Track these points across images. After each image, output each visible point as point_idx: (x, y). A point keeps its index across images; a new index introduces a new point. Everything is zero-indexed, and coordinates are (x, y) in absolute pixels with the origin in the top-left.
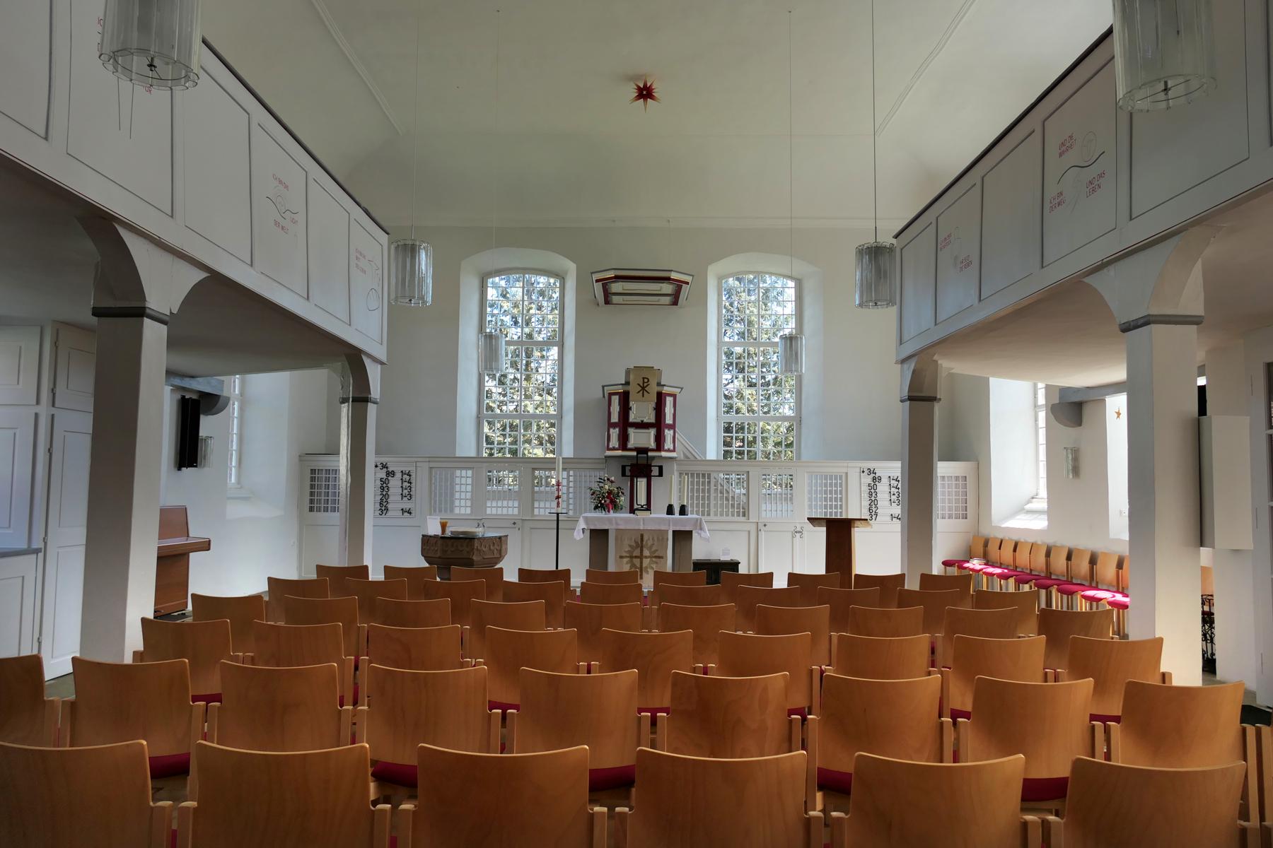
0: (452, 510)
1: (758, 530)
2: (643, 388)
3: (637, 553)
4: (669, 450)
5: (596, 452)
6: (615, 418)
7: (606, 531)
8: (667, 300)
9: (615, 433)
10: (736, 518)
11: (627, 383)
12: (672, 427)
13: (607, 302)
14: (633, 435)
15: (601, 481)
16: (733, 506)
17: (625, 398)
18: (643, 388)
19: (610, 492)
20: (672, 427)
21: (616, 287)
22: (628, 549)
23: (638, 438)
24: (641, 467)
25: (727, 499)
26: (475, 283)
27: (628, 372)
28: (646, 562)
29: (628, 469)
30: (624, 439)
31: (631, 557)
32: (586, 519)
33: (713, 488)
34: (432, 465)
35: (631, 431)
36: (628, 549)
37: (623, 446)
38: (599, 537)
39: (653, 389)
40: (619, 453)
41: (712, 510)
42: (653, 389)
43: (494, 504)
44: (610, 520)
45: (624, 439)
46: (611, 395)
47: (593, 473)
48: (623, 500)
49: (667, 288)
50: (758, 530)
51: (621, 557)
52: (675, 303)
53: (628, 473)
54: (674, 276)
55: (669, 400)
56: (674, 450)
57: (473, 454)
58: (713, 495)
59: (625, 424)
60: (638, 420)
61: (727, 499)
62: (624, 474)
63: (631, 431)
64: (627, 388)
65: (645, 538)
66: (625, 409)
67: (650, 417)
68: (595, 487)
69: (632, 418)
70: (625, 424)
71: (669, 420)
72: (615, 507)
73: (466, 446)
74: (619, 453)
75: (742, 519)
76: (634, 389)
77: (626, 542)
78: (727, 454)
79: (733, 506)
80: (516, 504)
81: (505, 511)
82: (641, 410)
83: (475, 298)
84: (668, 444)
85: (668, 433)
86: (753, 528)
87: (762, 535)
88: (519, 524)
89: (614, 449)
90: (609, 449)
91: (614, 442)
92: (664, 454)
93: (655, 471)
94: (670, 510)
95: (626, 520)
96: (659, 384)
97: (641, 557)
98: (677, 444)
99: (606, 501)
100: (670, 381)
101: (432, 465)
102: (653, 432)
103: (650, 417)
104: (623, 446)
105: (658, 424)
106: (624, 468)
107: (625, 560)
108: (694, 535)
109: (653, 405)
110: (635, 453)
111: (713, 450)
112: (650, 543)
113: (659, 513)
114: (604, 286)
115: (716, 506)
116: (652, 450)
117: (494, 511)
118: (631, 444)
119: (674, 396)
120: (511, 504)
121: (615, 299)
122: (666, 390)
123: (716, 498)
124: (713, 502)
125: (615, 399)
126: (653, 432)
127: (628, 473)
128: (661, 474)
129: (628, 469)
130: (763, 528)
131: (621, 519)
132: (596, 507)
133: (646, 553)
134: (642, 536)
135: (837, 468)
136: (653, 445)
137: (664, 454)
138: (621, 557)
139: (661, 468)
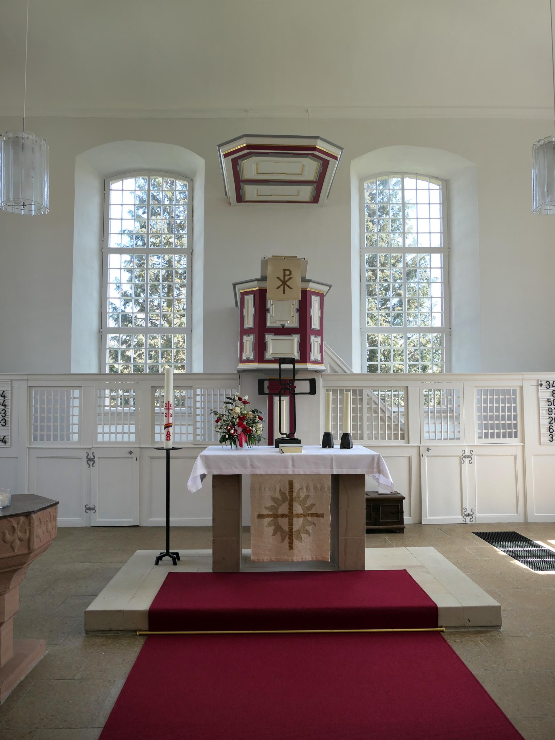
0: (68, 439)
1: (420, 456)
2: (284, 283)
3: (284, 509)
4: (316, 362)
5: (228, 365)
6: (249, 323)
7: (238, 478)
8: (306, 192)
9: (249, 341)
10: (393, 442)
11: (264, 279)
12: (319, 333)
13: (240, 198)
14: (273, 349)
15: (230, 401)
16: (389, 427)
17: (261, 297)
18: (284, 283)
19: (242, 418)
20: (319, 333)
21: (252, 167)
22: (270, 503)
23: (280, 347)
24: (280, 384)
25: (383, 420)
26: (96, 184)
27: (265, 262)
28: (298, 523)
29: (266, 384)
30: (260, 349)
31: (275, 516)
32: (207, 460)
33: (366, 407)
34: (31, 384)
35: (269, 338)
36: (270, 503)
37: (260, 356)
38: (226, 486)
39: (297, 285)
40: (255, 365)
41: (366, 433)
42: (297, 285)
43: (106, 429)
44: (242, 460)
45: (260, 349)
46: (243, 294)
47: (223, 391)
48: (261, 428)
49: (308, 168)
50: (420, 456)
51: (260, 516)
52: (315, 199)
53: (266, 391)
54: (320, 145)
55: (315, 300)
56: (321, 362)
57: (94, 370)
58: (366, 415)
59: (261, 329)
60: (278, 325)
61: (383, 420)
62: (261, 392)
63: (269, 338)
64: (263, 285)
65: (296, 486)
66: (262, 310)
67: (293, 322)
68: (223, 411)
69: (271, 322)
70: (261, 329)
71: (315, 325)
72: (250, 437)
73: (85, 362)
74: (255, 365)
75: (400, 442)
76: (271, 286)
77: (268, 494)
78: (372, 369)
79: (389, 427)
80: (133, 429)
81: (119, 438)
82: (281, 313)
83: (96, 201)
84: (315, 355)
85: (315, 341)
86: (413, 453)
87: (426, 461)
88: (136, 453)
89: (248, 361)
90: (242, 361)
91: (249, 353)
92: (310, 366)
93: (302, 386)
94: (327, 442)
95: (266, 460)
96: (304, 280)
97: (290, 516)
98: (323, 358)
99: (237, 431)
100: (316, 273)
101: (31, 384)
102: (296, 339)
103: (293, 322)
104: (260, 356)
105: (303, 330)
106: (261, 382)
107: (266, 521)
108: (367, 478)
109: (296, 305)
110: (276, 366)
111: (358, 364)
112: (303, 495)
113: (311, 449)
114: (235, 163)
115: (370, 428)
116: (298, 362)
117: (106, 438)
118: (269, 355)
119: (321, 295)
120: (126, 427)
121: (250, 191)
122: (312, 287)
123: (369, 419)
124: (366, 424)
125: (249, 300)
126: (296, 339)
127: (266, 391)
128: (313, 391)
129: (266, 384)
130: (426, 453)
131: (259, 458)
132: (223, 440)
133: (298, 509)
134: (291, 484)
135: (509, 381)
136: (296, 355)
137: (310, 366)
138: (260, 516)
139: (313, 383)
